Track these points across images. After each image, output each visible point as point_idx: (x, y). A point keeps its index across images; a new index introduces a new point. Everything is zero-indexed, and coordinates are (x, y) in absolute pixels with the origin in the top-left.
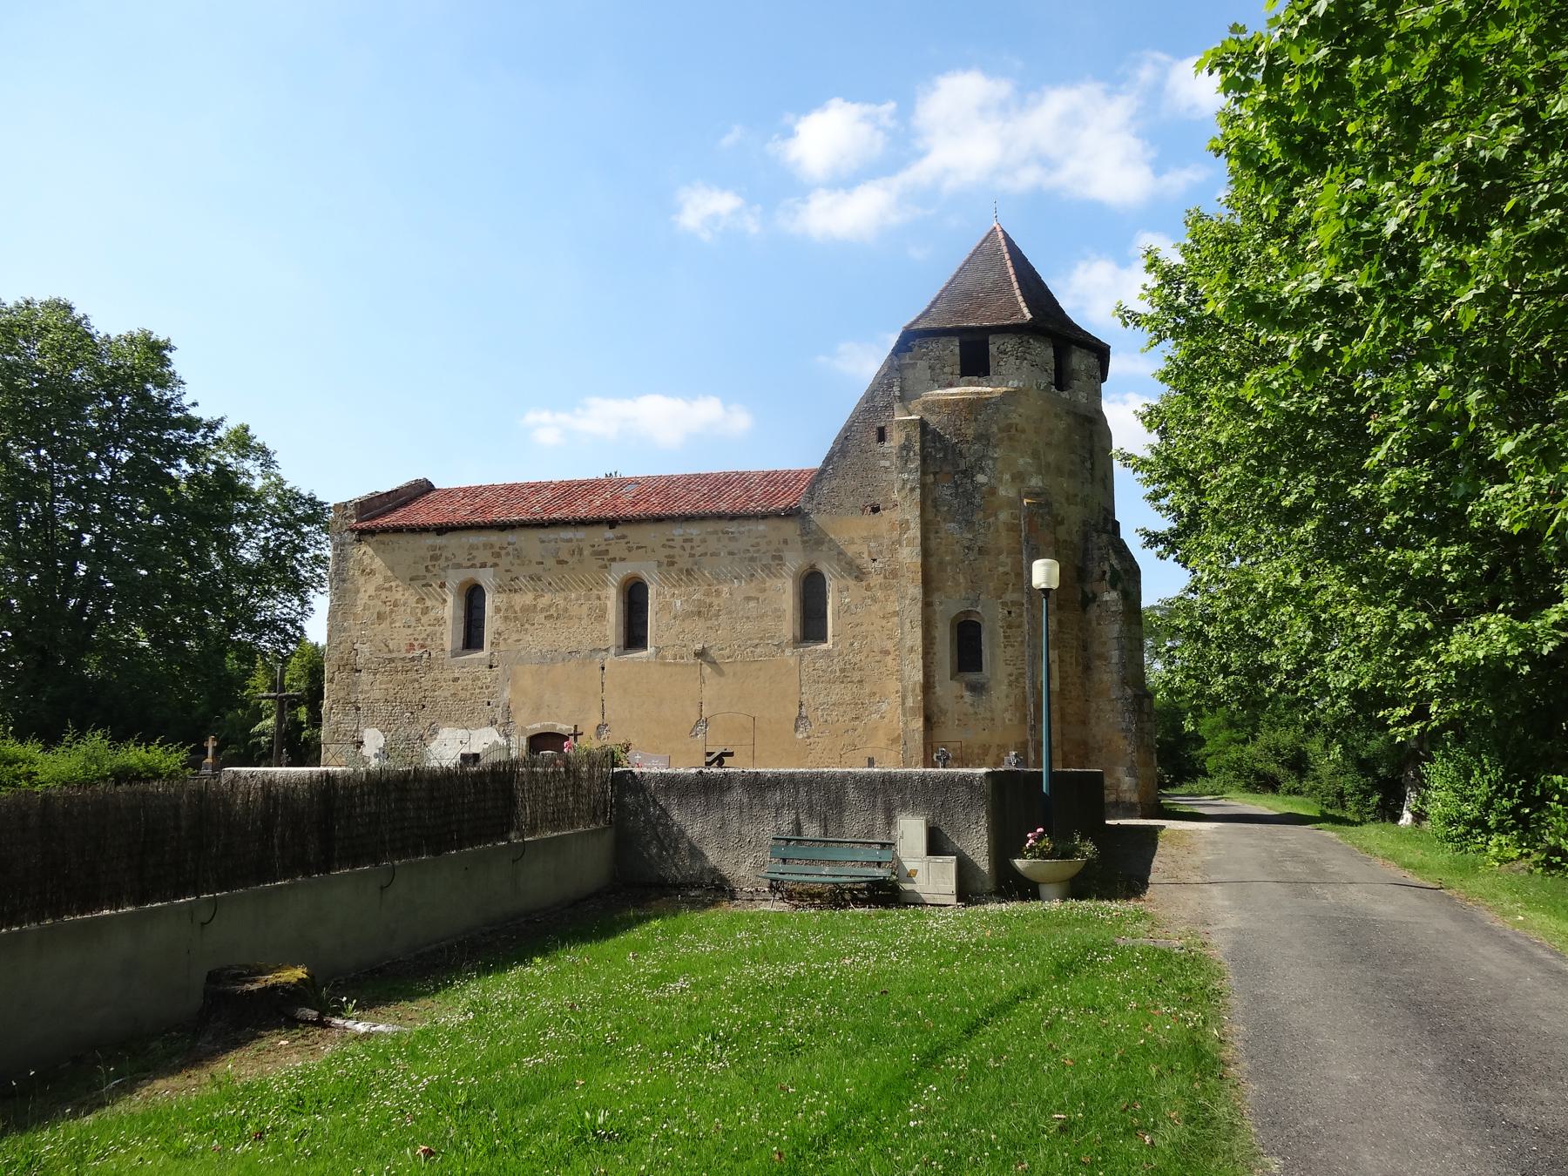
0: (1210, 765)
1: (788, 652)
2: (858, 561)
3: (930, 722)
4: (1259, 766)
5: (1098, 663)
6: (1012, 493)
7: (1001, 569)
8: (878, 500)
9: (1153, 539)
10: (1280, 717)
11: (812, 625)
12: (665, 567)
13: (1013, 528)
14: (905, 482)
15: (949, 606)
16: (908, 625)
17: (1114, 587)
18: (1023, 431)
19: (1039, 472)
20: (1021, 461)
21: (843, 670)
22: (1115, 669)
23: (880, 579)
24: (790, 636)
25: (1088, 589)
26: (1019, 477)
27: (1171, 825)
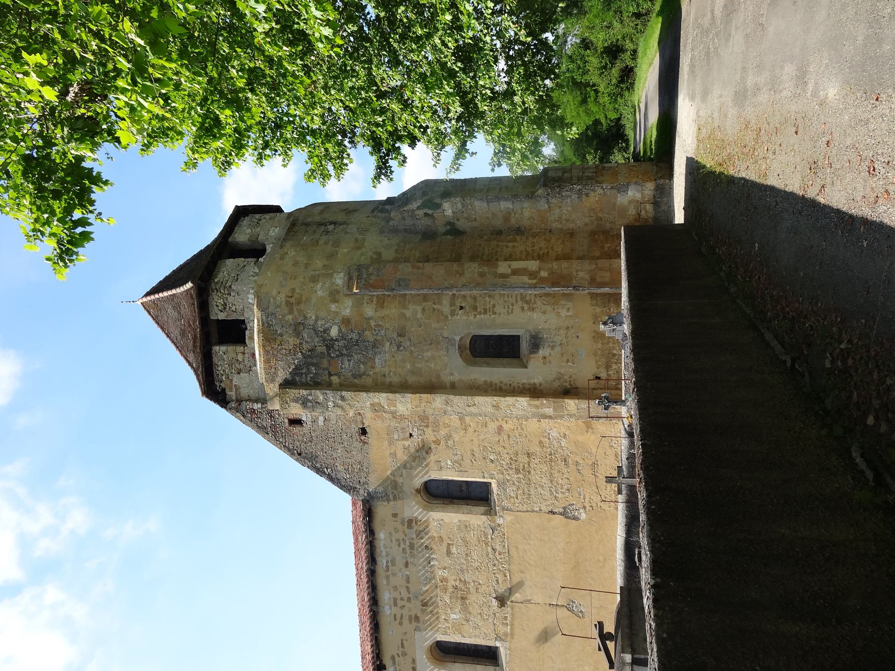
0: (613, 116)
1: (500, 521)
2: (412, 450)
3: (569, 392)
4: (614, 81)
5: (513, 221)
6: (348, 302)
7: (419, 315)
8: (355, 429)
9: (383, 171)
10: (579, 68)
11: (475, 495)
12: (420, 625)
13: (381, 303)
14: (336, 405)
15: (455, 367)
16: (472, 409)
17: (438, 206)
18: (293, 290)
19: (331, 275)
20: (320, 293)
21: (517, 471)
22: (518, 206)
23: (429, 431)
24: (484, 518)
25: (442, 230)
26: (334, 296)
27: (685, 146)
